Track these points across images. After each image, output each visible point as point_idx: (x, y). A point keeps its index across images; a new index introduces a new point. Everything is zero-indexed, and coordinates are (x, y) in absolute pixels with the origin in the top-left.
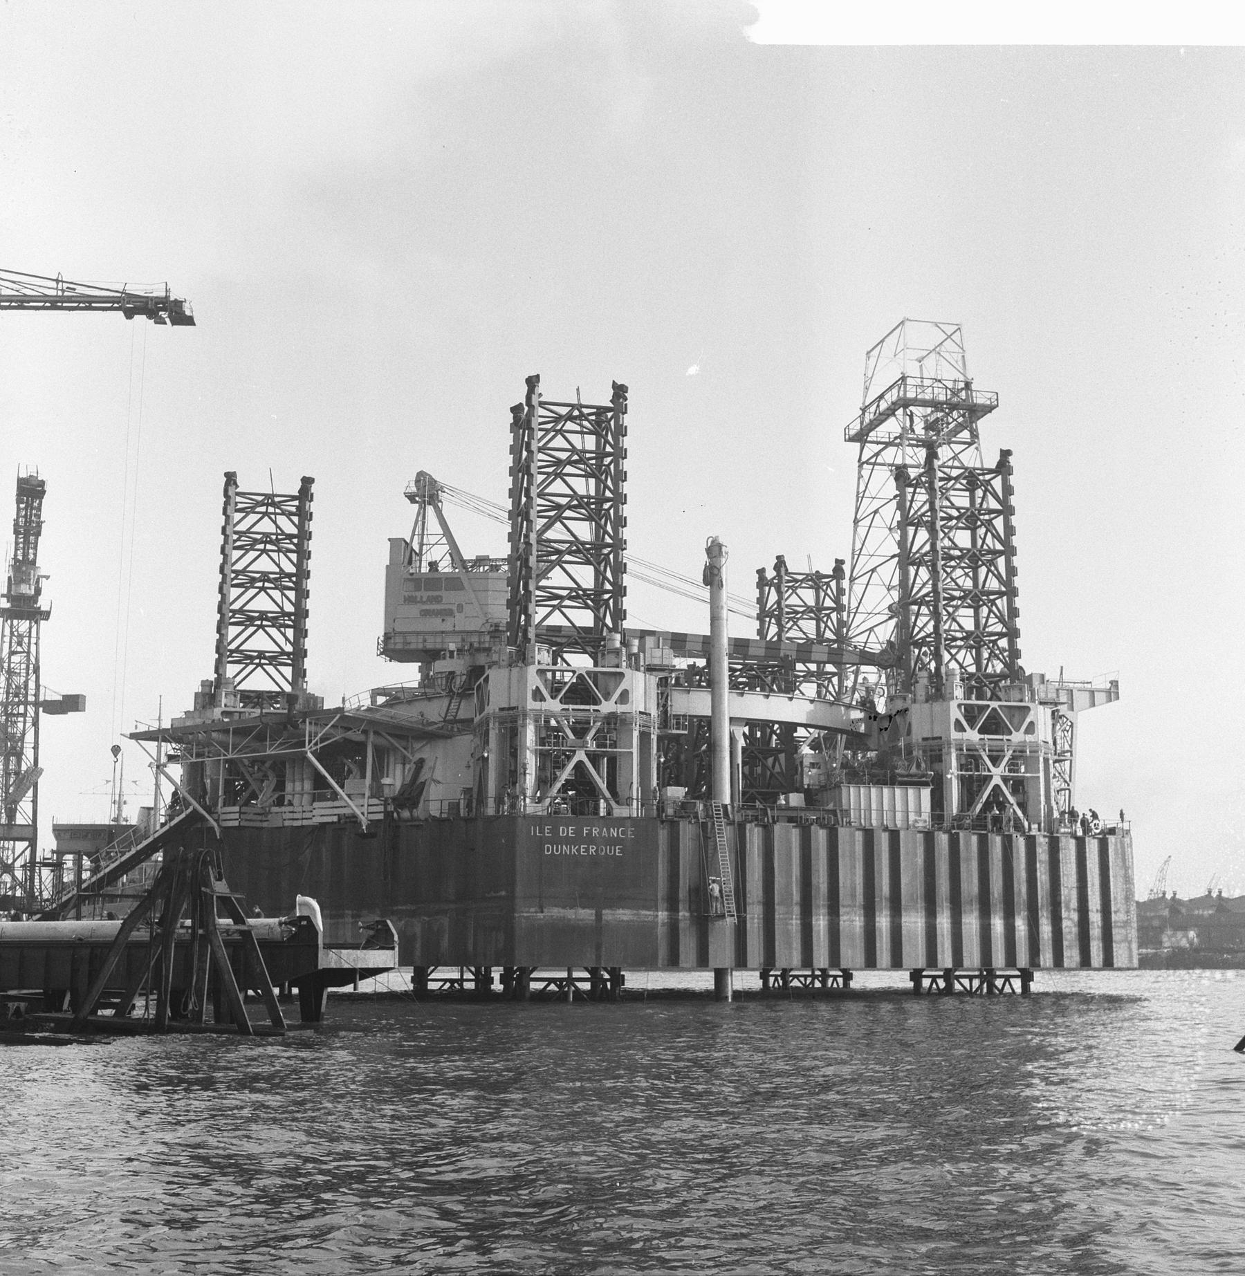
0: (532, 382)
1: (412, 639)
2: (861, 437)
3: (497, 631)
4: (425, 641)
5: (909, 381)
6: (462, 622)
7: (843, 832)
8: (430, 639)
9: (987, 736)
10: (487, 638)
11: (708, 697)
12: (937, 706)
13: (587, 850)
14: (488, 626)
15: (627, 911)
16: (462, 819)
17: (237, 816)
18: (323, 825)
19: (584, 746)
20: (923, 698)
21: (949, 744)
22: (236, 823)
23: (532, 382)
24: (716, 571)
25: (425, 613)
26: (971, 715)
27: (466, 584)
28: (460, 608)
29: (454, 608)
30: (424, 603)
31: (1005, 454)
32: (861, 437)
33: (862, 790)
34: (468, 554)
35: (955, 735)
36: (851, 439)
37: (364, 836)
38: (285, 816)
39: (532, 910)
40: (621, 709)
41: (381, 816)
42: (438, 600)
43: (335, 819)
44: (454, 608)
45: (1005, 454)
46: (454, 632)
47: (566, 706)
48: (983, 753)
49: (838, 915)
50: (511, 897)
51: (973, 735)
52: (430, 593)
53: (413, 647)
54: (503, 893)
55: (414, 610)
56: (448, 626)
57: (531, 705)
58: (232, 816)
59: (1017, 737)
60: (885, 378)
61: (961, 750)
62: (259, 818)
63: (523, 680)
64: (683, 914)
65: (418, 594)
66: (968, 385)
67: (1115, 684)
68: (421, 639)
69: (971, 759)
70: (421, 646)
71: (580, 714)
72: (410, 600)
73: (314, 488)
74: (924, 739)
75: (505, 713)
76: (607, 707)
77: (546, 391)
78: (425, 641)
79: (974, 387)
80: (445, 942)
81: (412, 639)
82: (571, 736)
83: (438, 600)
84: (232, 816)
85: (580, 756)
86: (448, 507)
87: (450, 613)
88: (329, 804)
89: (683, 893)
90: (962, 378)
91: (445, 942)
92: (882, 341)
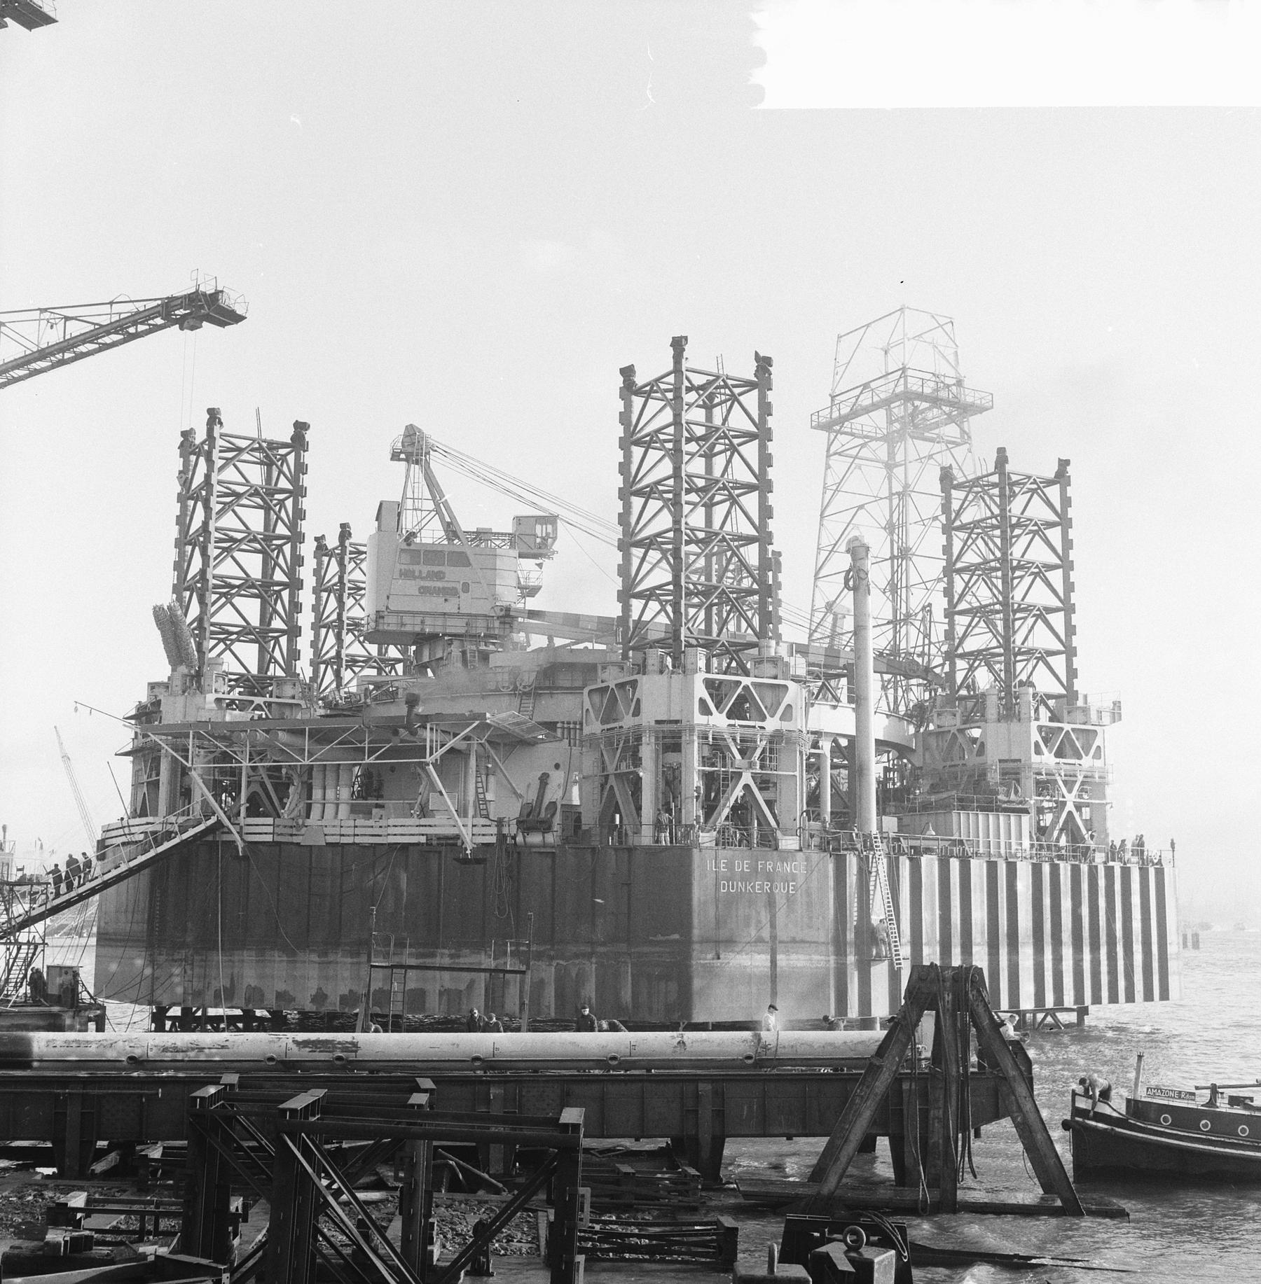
0: (678, 345)
1: (407, 620)
2: (831, 426)
3: (508, 616)
4: (422, 622)
5: (909, 372)
6: (468, 604)
7: (974, 863)
8: (428, 621)
9: (1062, 760)
10: (497, 624)
11: (852, 716)
12: (1015, 726)
13: (762, 888)
14: (497, 610)
15: (801, 957)
16: (611, 847)
17: (270, 829)
18: (405, 846)
19: (751, 765)
20: (995, 716)
21: (692, 730)
22: (269, 838)
23: (678, 345)
24: (862, 575)
25: (424, 591)
26: (1048, 735)
27: (471, 558)
28: (466, 587)
29: (459, 587)
30: (422, 579)
31: (1064, 464)
32: (831, 426)
33: (991, 817)
34: (467, 524)
35: (699, 719)
36: (820, 427)
37: (465, 861)
38: (327, 831)
39: (709, 956)
40: (786, 726)
41: (493, 840)
42: (439, 576)
43: (423, 840)
44: (459, 587)
45: (1064, 464)
46: (459, 615)
47: (732, 722)
48: (1058, 778)
49: (971, 954)
50: (686, 943)
51: (719, 720)
52: (429, 568)
53: (408, 628)
54: (676, 936)
55: (412, 586)
56: (450, 607)
57: (699, 719)
58: (265, 829)
59: (1087, 761)
60: (868, 366)
61: (707, 738)
62: (289, 831)
63: (688, 691)
64: (851, 959)
65: (416, 568)
66: (959, 383)
67: (1117, 705)
68: (418, 620)
69: (717, 749)
70: (417, 629)
71: (1068, 767)
72: (406, 575)
73: (309, 436)
74: (658, 722)
75: (666, 727)
76: (772, 724)
77: (693, 357)
78: (422, 622)
79: (966, 384)
80: (590, 990)
81: (407, 620)
82: (738, 756)
83: (439, 576)
84: (265, 829)
85: (746, 778)
86: (437, 464)
87: (453, 592)
88: (415, 821)
89: (850, 936)
90: (952, 373)
91: (590, 990)
92: (868, 325)
